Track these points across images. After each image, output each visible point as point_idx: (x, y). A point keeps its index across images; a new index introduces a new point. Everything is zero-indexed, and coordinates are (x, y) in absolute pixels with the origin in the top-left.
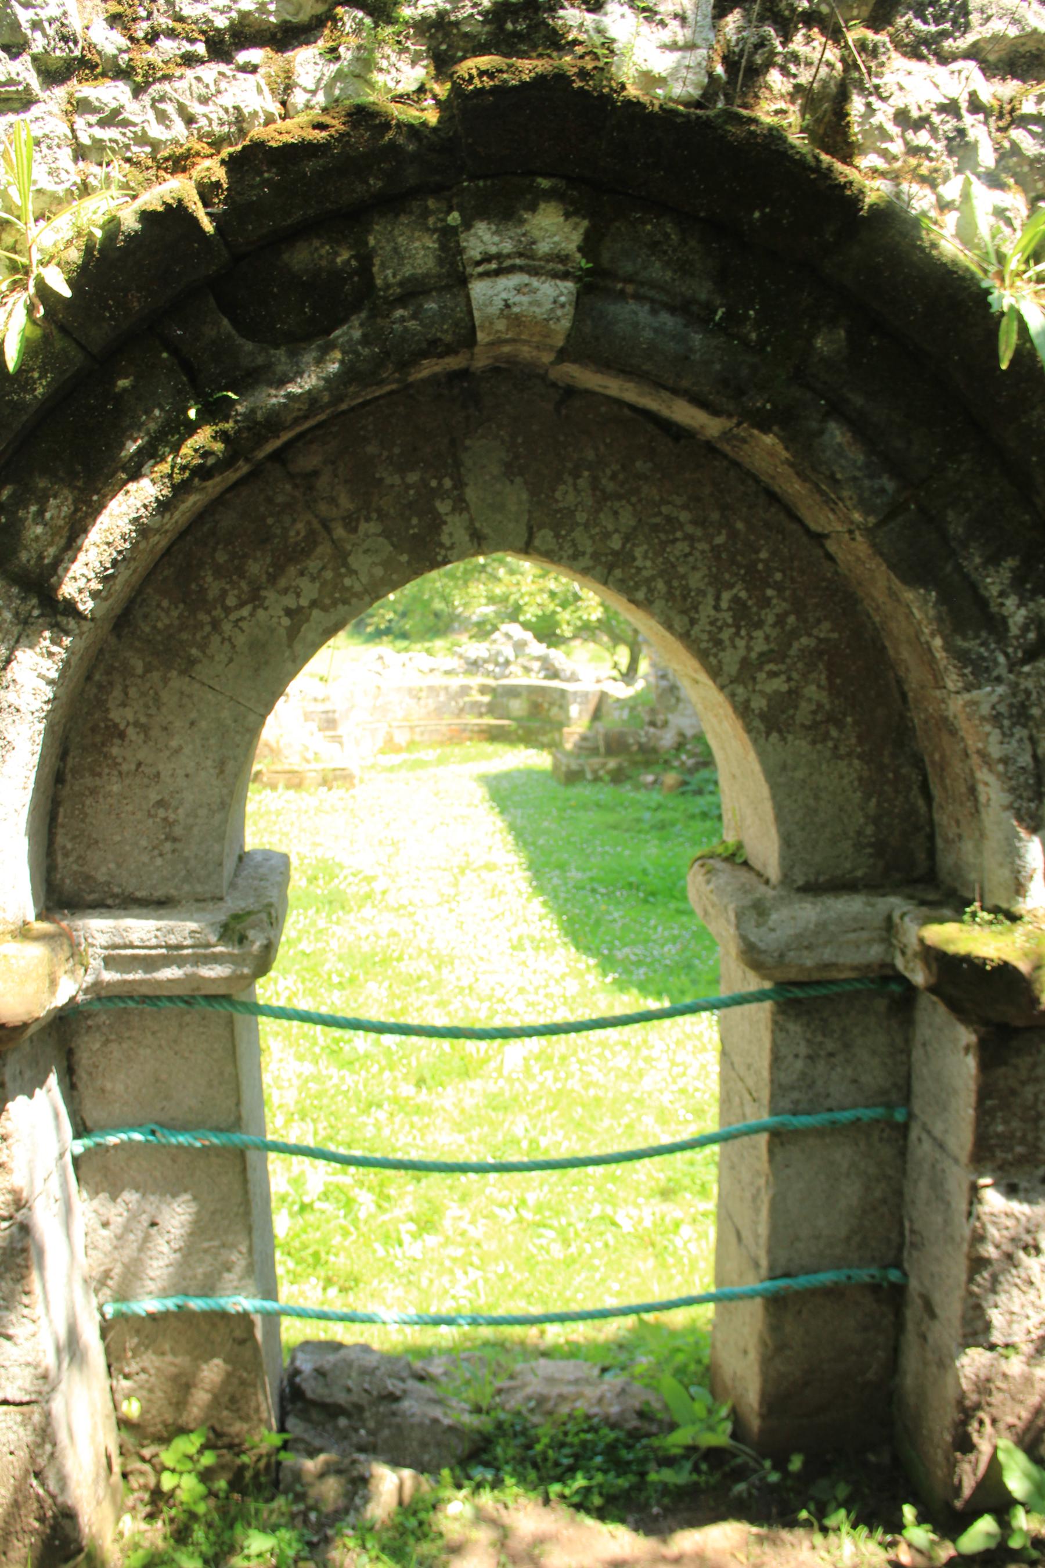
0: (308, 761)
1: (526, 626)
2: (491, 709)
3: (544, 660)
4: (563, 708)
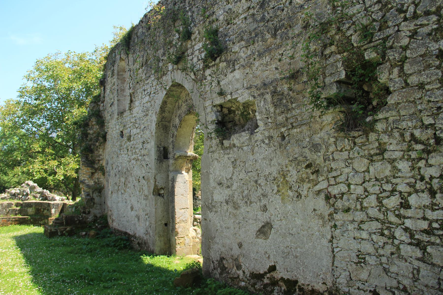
1: (35, 181)
2: (20, 212)
3: (42, 193)
4: (49, 210)
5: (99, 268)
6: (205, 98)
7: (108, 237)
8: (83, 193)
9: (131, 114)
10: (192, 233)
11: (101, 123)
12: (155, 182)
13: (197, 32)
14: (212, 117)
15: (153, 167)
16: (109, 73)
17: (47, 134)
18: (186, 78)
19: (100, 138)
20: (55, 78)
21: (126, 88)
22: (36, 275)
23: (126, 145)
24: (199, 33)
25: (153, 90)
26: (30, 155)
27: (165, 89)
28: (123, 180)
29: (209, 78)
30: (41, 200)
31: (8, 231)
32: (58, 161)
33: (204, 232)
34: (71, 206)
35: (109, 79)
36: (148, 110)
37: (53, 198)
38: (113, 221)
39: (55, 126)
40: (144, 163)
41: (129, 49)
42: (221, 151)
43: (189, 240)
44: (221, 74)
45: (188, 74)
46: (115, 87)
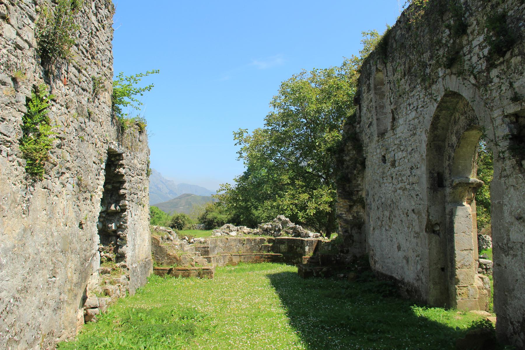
0: (192, 265)
2: (273, 249)
4: (303, 248)
5: (361, 317)
6: (493, 107)
7: (370, 281)
8: (340, 228)
9: (395, 134)
10: (477, 282)
11: (359, 147)
12: (429, 216)
13: (475, 23)
14: (503, 131)
15: (426, 198)
16: (364, 88)
17: (297, 163)
18: (464, 84)
19: (358, 165)
20: (300, 100)
21: (386, 104)
22: (293, 317)
23: (390, 172)
24: (478, 24)
25: (420, 103)
26: (279, 188)
27: (436, 100)
28: (387, 213)
29: (496, 80)
30: (294, 236)
31: (261, 269)
32: (309, 194)
33: (497, 282)
34: (328, 244)
35: (365, 95)
36: (415, 128)
37: (306, 234)
38: (375, 262)
39: (305, 155)
40: (413, 193)
41: (386, 57)
42: (520, 175)
43: (474, 291)
44: (514, 73)
45: (466, 79)
46: (373, 104)
